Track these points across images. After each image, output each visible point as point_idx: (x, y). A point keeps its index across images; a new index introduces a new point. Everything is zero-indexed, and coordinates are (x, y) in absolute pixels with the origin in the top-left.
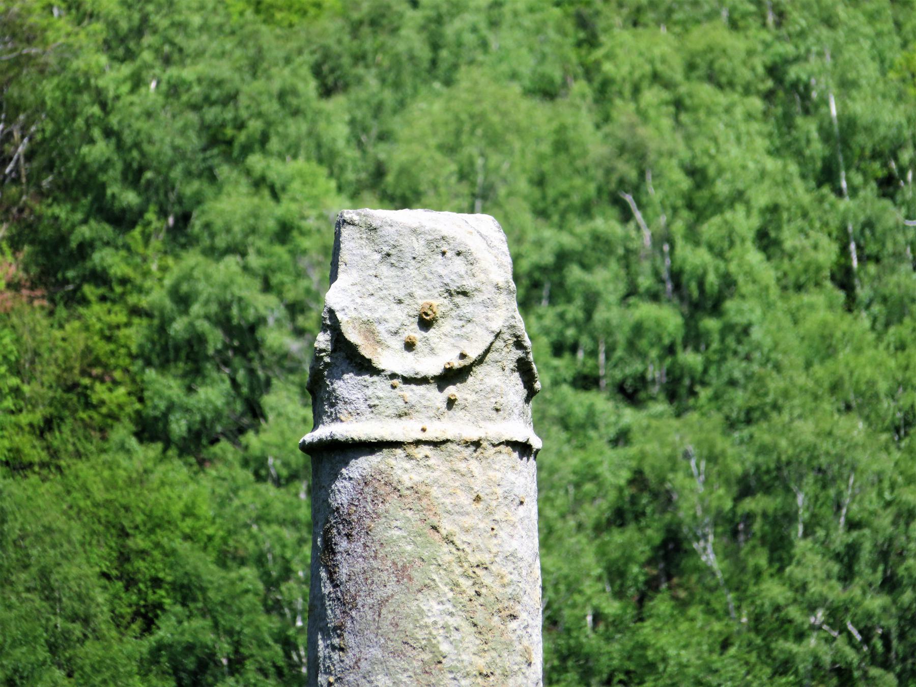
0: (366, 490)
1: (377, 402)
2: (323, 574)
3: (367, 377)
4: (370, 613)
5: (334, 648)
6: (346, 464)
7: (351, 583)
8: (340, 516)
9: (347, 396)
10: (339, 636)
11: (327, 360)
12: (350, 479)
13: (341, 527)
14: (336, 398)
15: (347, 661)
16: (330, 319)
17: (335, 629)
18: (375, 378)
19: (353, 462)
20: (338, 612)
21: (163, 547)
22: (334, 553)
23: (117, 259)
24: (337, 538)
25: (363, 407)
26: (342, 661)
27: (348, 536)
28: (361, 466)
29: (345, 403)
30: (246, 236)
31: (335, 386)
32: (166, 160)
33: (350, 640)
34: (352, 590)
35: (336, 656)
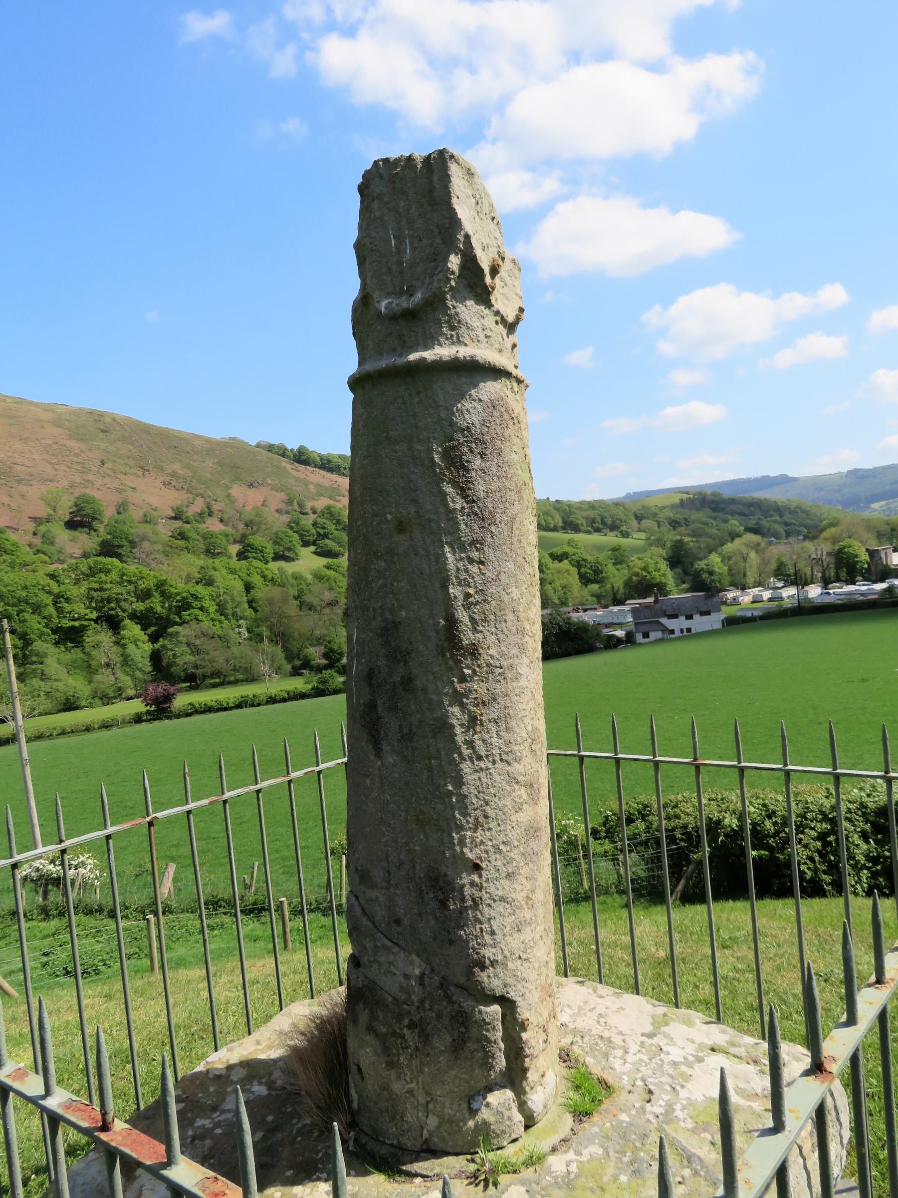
0: (495, 413)
2: (449, 489)
4: (505, 528)
5: (471, 561)
6: (475, 386)
7: (489, 500)
8: (472, 435)
9: (469, 322)
10: (477, 550)
11: (453, 283)
12: (480, 400)
13: (474, 446)
14: (459, 322)
15: (488, 574)
16: (464, 243)
17: (473, 543)
18: (487, 311)
19: (459, 216)
20: (476, 527)
21: (285, 649)
22: (468, 471)
23: (82, 591)
24: (470, 456)
26: (484, 574)
27: (482, 455)
28: (489, 389)
29: (468, 328)
30: (316, 941)
31: (458, 310)
32: (32, 885)
33: (489, 553)
34: (490, 506)
35: (474, 569)
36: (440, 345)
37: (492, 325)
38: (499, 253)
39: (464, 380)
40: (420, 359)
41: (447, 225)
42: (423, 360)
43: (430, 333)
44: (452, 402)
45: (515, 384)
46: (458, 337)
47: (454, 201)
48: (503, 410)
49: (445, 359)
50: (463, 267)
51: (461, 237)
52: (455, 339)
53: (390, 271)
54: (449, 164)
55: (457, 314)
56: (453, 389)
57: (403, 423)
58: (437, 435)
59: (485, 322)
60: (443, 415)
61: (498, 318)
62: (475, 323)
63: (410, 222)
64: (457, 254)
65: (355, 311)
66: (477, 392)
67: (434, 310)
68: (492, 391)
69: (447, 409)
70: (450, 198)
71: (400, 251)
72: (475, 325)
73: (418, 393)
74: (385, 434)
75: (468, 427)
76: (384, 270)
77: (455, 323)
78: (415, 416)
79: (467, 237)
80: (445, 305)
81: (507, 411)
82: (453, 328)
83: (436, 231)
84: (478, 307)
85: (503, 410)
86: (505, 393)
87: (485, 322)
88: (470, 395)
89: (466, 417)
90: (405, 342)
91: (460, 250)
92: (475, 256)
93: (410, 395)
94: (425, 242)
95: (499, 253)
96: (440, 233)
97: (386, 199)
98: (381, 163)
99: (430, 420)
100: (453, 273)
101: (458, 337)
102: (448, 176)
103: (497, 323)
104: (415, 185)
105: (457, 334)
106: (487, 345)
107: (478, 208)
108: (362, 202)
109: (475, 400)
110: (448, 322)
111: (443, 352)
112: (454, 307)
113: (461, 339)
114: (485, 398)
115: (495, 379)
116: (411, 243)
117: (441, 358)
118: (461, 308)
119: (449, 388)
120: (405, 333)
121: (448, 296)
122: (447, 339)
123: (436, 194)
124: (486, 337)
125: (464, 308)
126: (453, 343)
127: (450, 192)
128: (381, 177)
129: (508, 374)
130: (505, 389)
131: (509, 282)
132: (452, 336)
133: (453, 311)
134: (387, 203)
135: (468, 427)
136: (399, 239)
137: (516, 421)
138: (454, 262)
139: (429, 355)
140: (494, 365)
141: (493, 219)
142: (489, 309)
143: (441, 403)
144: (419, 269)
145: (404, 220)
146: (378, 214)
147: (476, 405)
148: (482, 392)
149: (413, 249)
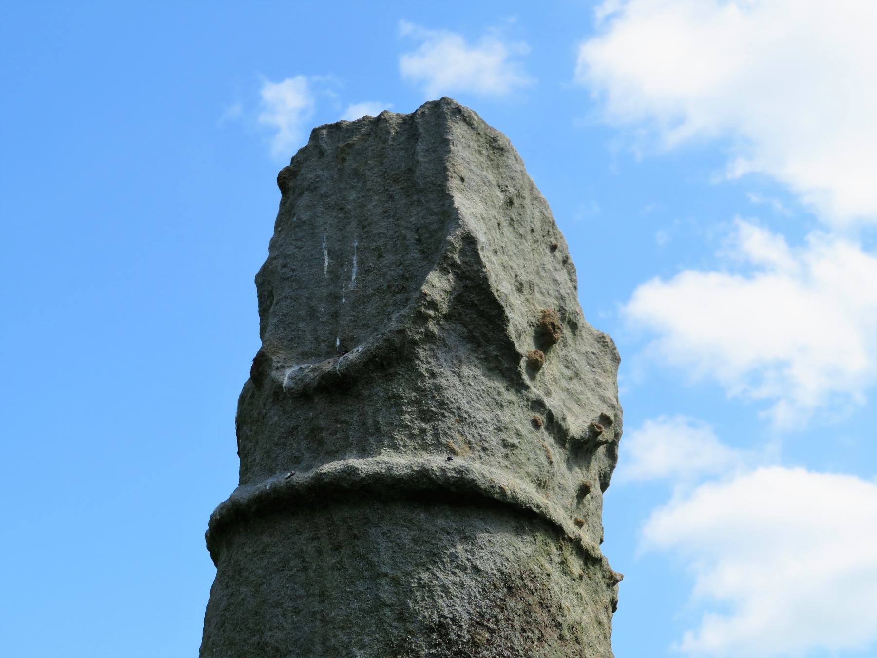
0: (511, 603)
1: (515, 440)
3: (499, 385)
9: (466, 407)
12: (477, 570)
14: (442, 404)
16: (462, 252)
18: (510, 396)
25: (494, 441)
28: (502, 549)
29: (461, 420)
31: (441, 381)
36: (394, 447)
37: (526, 428)
38: (562, 310)
39: (441, 522)
40: (343, 471)
41: (434, 226)
42: (352, 471)
43: (376, 423)
44: (410, 568)
45: (576, 565)
46: (436, 435)
47: (453, 184)
48: (533, 600)
49: (396, 472)
50: (458, 299)
51: (454, 238)
52: (429, 439)
53: (312, 313)
54: (450, 123)
55: (438, 388)
56: (415, 541)
57: (297, 612)
58: (367, 640)
59: (505, 416)
60: (386, 594)
61: (541, 418)
62: (481, 412)
63: (364, 225)
64: (445, 271)
65: (243, 400)
66: (471, 551)
67: (389, 378)
68: (508, 553)
69: (395, 581)
70: (446, 178)
71: (335, 277)
72: (479, 416)
73: (337, 548)
74: (255, 639)
75: (441, 625)
76: (302, 313)
77: (433, 409)
78: (323, 596)
79: (470, 241)
80: (413, 369)
81: (544, 605)
82: (425, 416)
83: (411, 236)
84: (490, 383)
85: (533, 600)
86: (541, 566)
87: (505, 416)
88: (454, 557)
89: (440, 602)
90: (321, 442)
91: (453, 265)
92: (486, 279)
93: (319, 552)
94: (389, 258)
95: (562, 310)
96: (419, 241)
97: (324, 189)
98: (325, 132)
99: (355, 605)
100: (433, 305)
101: (436, 435)
102: (446, 143)
103: (536, 424)
104: (382, 164)
105: (435, 428)
106: (504, 462)
107: (513, 213)
108: (282, 204)
109: (464, 569)
110: (416, 402)
111: (399, 460)
112: (433, 375)
113: (443, 440)
114: (488, 567)
115: (519, 531)
116: (361, 263)
117: (389, 469)
118: (447, 379)
119: (406, 537)
120: (323, 423)
121: (422, 353)
122: (412, 436)
123: (418, 173)
124: (505, 445)
125: (455, 380)
126: (425, 447)
127: (446, 169)
128: (322, 154)
129: (555, 530)
130: (544, 561)
131: (588, 376)
132: (423, 431)
133: (429, 382)
134: (324, 196)
135: (441, 625)
136: (339, 257)
137: (568, 635)
138: (438, 285)
139: (364, 465)
140: (515, 499)
141: (553, 248)
142: (518, 391)
143: (385, 569)
144: (371, 309)
145: (354, 223)
146: (305, 217)
147: (467, 580)
148: (483, 553)
149: (365, 271)
